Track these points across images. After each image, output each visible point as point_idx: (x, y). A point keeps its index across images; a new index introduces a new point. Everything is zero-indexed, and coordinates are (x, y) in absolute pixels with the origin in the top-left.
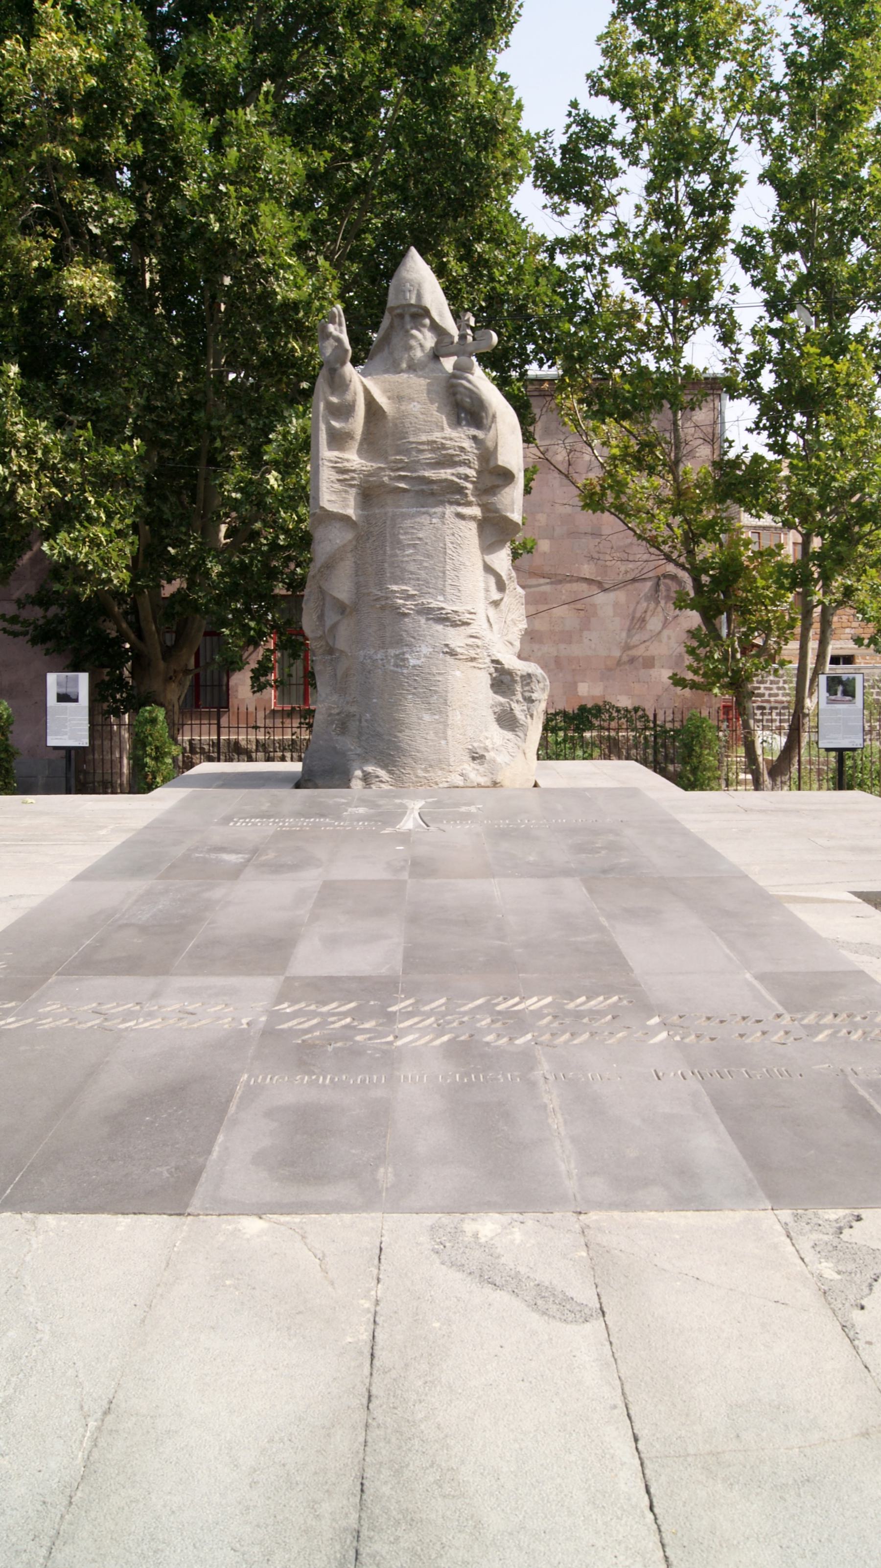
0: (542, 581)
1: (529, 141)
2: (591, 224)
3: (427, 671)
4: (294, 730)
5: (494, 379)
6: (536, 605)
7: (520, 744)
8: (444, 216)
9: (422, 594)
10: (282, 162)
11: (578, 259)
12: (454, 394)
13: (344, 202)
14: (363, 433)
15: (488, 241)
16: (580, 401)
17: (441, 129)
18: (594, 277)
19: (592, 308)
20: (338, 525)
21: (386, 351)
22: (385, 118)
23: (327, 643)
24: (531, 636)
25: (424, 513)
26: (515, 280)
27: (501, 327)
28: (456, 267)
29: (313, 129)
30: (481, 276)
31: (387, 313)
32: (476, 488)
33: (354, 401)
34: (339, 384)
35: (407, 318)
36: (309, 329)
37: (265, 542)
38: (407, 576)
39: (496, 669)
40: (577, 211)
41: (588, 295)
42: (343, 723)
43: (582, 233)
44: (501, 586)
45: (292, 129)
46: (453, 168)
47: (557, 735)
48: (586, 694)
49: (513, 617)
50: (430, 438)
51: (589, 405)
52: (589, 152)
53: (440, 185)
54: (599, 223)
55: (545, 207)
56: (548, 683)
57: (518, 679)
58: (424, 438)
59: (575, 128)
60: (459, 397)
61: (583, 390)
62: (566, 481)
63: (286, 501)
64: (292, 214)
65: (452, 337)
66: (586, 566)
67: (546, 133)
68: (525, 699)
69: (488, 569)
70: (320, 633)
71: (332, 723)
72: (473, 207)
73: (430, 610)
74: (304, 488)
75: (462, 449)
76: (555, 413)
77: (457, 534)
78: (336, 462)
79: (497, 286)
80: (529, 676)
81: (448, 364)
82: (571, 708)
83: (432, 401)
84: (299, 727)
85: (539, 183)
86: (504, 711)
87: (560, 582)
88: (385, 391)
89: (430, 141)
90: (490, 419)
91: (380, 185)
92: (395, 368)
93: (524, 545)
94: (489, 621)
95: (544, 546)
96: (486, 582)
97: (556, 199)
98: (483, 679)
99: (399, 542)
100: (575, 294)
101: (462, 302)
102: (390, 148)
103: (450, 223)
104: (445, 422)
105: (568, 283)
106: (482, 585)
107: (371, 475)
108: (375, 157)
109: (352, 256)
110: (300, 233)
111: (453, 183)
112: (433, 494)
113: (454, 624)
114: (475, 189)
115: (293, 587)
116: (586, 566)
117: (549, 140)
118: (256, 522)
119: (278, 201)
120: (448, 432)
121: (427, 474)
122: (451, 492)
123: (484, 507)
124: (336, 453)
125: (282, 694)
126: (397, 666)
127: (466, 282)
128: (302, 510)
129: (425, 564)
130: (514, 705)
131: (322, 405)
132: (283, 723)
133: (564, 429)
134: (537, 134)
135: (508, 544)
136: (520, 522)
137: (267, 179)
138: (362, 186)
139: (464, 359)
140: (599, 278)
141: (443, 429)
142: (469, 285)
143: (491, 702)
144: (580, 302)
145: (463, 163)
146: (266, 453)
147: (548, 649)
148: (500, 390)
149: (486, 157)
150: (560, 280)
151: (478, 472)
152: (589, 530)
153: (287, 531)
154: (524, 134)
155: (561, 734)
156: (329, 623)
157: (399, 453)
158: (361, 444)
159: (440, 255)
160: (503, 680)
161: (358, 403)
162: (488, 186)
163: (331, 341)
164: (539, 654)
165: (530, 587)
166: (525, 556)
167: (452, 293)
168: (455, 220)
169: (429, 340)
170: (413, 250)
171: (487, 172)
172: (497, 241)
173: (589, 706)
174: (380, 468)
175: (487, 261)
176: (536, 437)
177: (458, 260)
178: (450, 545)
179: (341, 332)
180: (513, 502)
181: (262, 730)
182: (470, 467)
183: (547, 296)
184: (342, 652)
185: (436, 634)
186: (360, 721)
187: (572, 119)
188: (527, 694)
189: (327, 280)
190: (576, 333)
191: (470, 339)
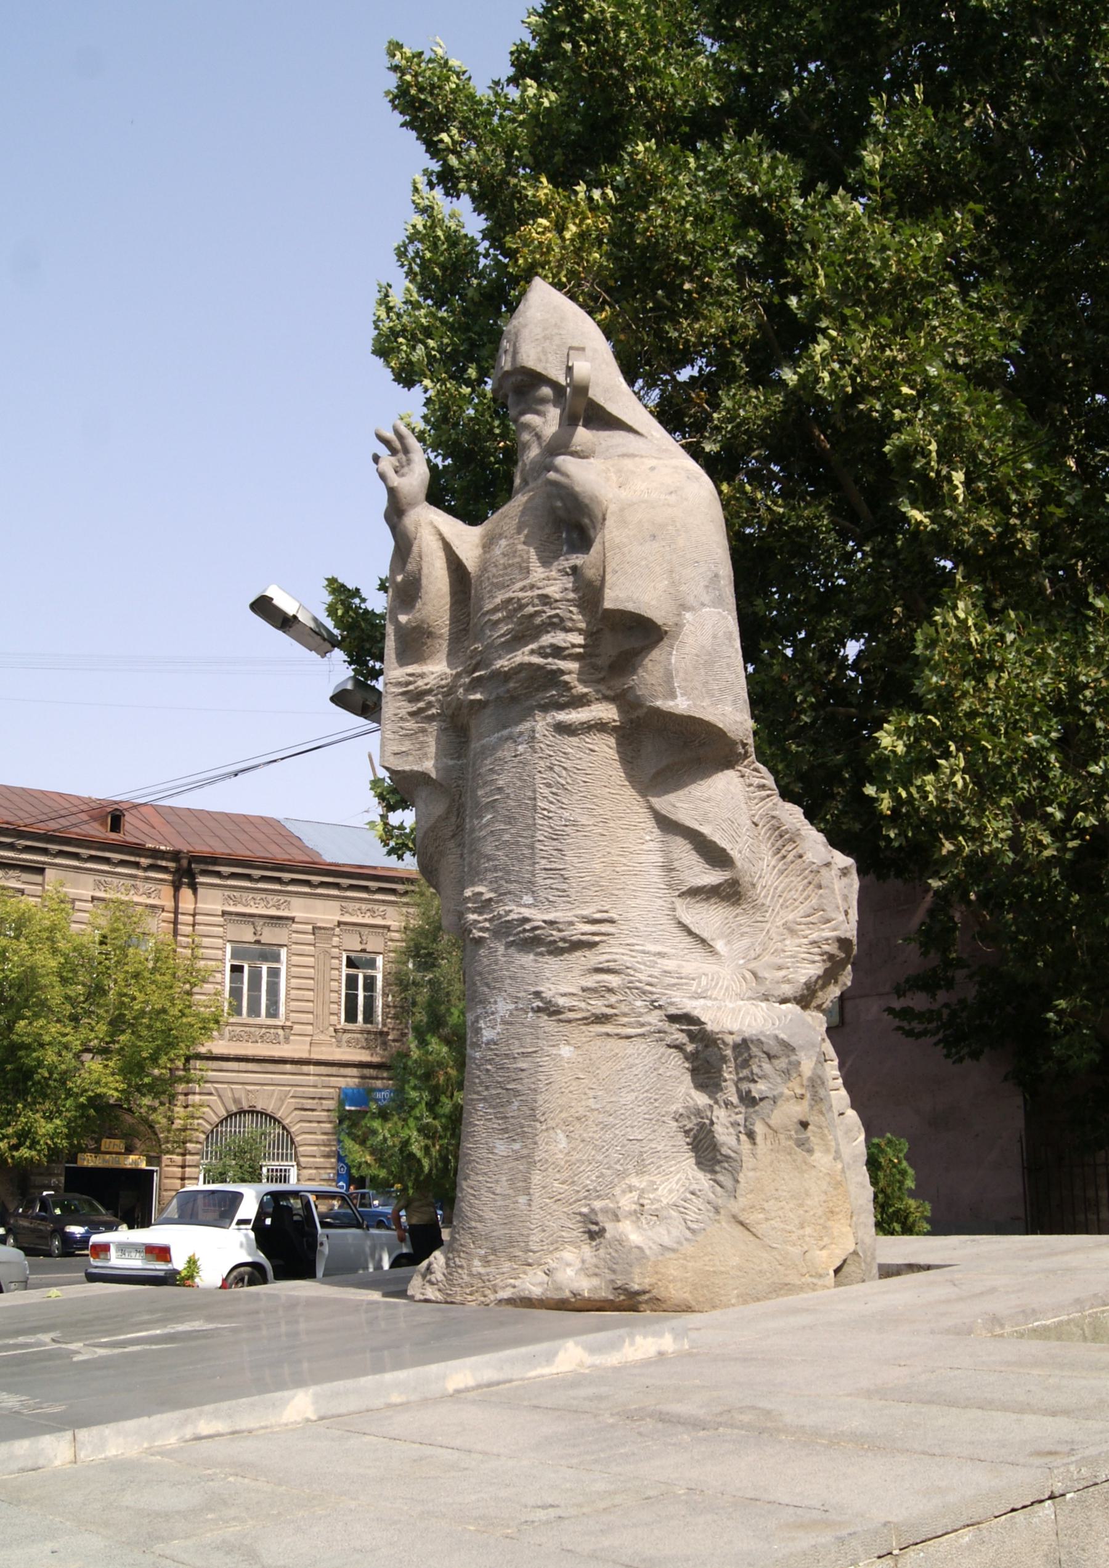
3: (504, 1050)
57: (729, 1052)
75: (545, 599)
113: (556, 950)
129: (506, 837)
178: (546, 791)
188: (744, 1086)
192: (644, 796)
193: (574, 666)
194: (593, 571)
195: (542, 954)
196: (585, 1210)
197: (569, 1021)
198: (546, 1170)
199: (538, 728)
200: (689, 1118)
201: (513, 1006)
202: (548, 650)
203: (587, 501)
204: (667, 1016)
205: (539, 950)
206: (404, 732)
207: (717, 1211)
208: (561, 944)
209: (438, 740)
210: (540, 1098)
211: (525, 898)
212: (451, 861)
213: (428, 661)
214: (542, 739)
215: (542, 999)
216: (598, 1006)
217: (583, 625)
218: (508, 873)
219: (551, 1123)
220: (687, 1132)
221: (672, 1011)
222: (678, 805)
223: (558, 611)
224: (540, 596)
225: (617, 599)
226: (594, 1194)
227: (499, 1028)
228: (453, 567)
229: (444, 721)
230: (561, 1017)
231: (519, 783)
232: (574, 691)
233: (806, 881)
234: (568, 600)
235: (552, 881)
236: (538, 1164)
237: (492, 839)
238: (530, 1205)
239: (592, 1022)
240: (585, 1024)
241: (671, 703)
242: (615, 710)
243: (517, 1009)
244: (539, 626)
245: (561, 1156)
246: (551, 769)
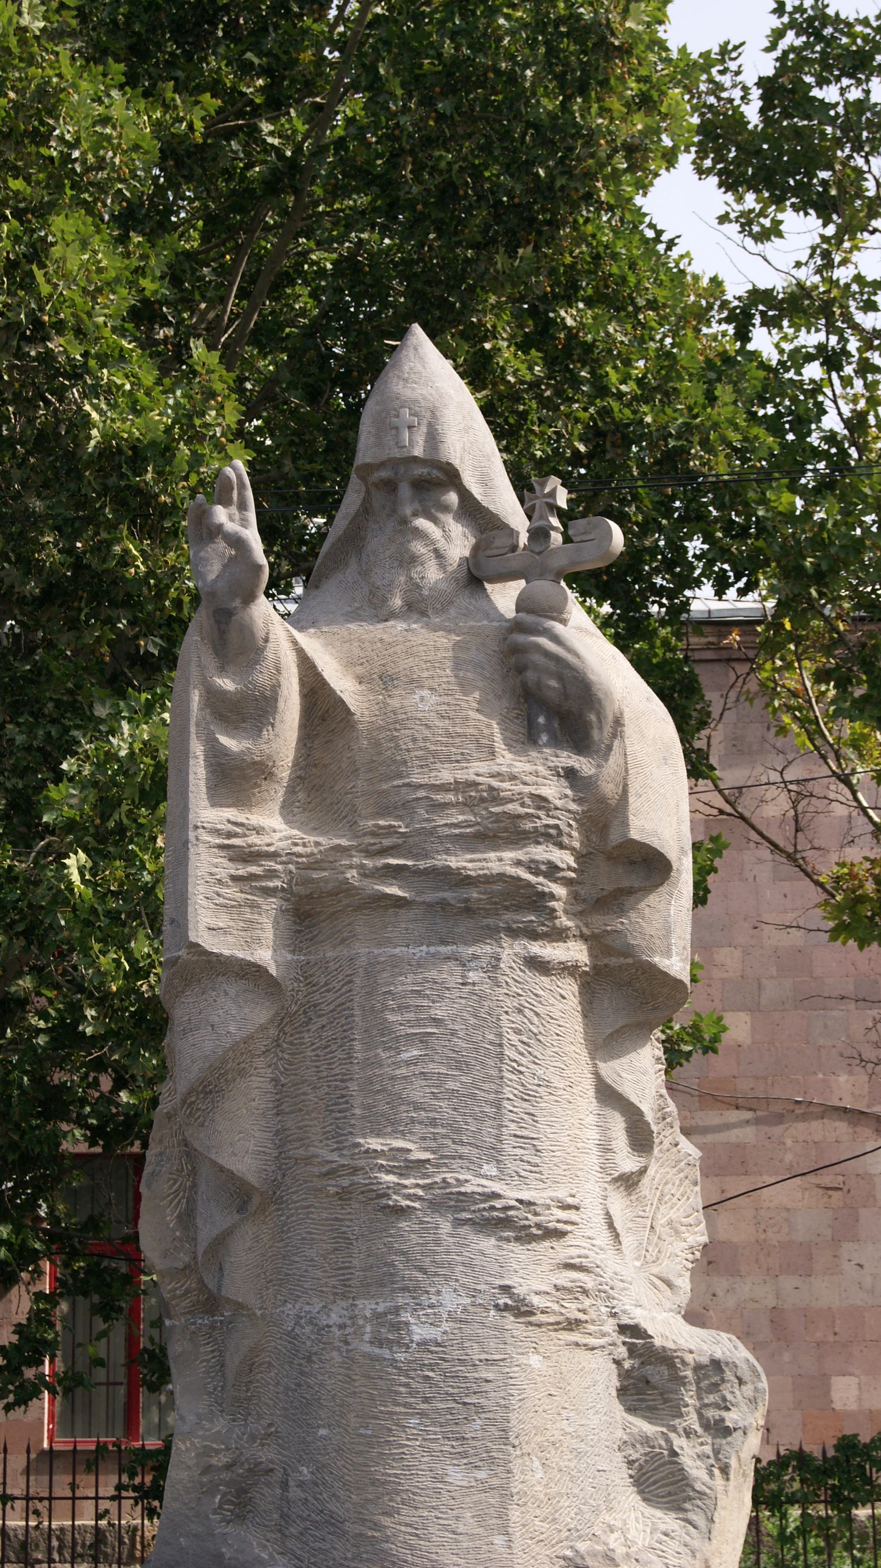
0: (734, 1116)
1: (689, 70)
2: (837, 259)
3: (456, 1354)
4: (104, 1505)
5: (605, 624)
6: (725, 1181)
7: (696, 1544)
8: (484, 245)
9: (443, 1160)
10: (105, 120)
11: (811, 339)
12: (520, 670)
13: (242, 210)
14: (296, 764)
15: (590, 302)
16: (821, 676)
17: (477, 47)
18: (847, 382)
19: (843, 453)
20: (233, 988)
21: (353, 566)
22: (339, 18)
23: (201, 1281)
24: (712, 1261)
25: (448, 958)
26: (659, 389)
27: (623, 502)
28: (518, 365)
29: (171, 47)
30: (576, 382)
31: (354, 480)
32: (575, 897)
33: (276, 687)
34: (238, 647)
35: (405, 491)
36: (166, 511)
37: (42, 1024)
38: (405, 1113)
39: (632, 1350)
40: (802, 229)
41: (831, 422)
42: (242, 1492)
43: (817, 279)
44: (641, 1138)
45: (121, 45)
46: (506, 135)
47: (784, 1516)
48: (853, 1406)
49: (673, 1214)
50: (461, 776)
51: (843, 684)
52: (830, 94)
53: (477, 174)
54: (856, 256)
55: (724, 219)
56: (764, 1384)
58: (446, 775)
59: (791, 39)
60: (531, 676)
61: (828, 651)
62: (788, 869)
63: (103, 922)
64: (123, 239)
65: (513, 533)
66: (843, 1078)
67: (724, 50)
68: (706, 1425)
69: (608, 1095)
70: (184, 1258)
71: (212, 1490)
72: (555, 224)
73: (463, 1200)
74: (149, 890)
75: (541, 801)
76: (759, 703)
77: (533, 1008)
78: (230, 835)
79: (615, 405)
80: (716, 1365)
81: (505, 597)
82: (819, 1443)
83: (465, 687)
84: (117, 1498)
85: (708, 163)
86: (652, 1457)
87: (779, 1119)
88: (349, 663)
89: (450, 75)
90: (608, 730)
91: (331, 175)
92: (376, 609)
93: (695, 1033)
94: (611, 1226)
95: (739, 1028)
96: (604, 1129)
97: (750, 200)
98: (596, 1375)
99: (385, 1029)
100: (804, 420)
101: (530, 444)
102: (355, 87)
103: (500, 260)
104: (498, 737)
105: (783, 396)
106: (593, 1135)
107: (315, 864)
108: (318, 107)
109: (265, 337)
110: (145, 283)
111: (507, 169)
112: (468, 910)
113: (525, 1236)
114: (560, 182)
115: (105, 1136)
116: (843, 1078)
117: (733, 66)
118: (20, 975)
119: (90, 209)
120: (507, 760)
121: (453, 862)
122: (516, 907)
123: (596, 942)
124: (230, 813)
125: (71, 1409)
126: (379, 1342)
127: (539, 398)
128: (141, 947)
129: (451, 1085)
130: (679, 1442)
131: (196, 698)
132: (73, 1486)
133: (780, 742)
134: (706, 55)
135: (658, 1033)
136: (686, 979)
137: (66, 158)
138: (288, 175)
139: (543, 586)
140: (858, 384)
141: (493, 754)
142: (544, 403)
143: (620, 1434)
144: (814, 439)
145: (529, 125)
146: (50, 805)
147: (753, 1290)
148: (624, 649)
149: (585, 111)
150: (765, 389)
151: (579, 857)
152: (849, 988)
153: (102, 1001)
154: (674, 55)
155: (795, 1512)
156: (206, 1233)
157: (385, 811)
158: (291, 790)
159: (475, 335)
160: (648, 1378)
161: (284, 691)
162: (590, 176)
163: (221, 544)
164: (731, 1302)
165: (705, 1130)
166: (697, 1057)
167: (504, 417)
168: (512, 253)
169: (457, 541)
170: (417, 332)
171: (587, 144)
172: (613, 300)
173: (865, 1438)
174: (337, 848)
175: (589, 348)
176: (713, 761)
177: (519, 347)
178: (514, 1038)
179: (244, 523)
180: (668, 928)
181: (19, 1505)
182: (561, 846)
183: (736, 428)
184: (240, 1306)
185: (478, 1261)
186: (285, 1485)
187: (786, 19)
188: (712, 1414)
189: (213, 395)
190: (807, 514)
191: (556, 538)
192: (593, 1058)
193: (560, 891)
194: (611, 786)
195: (508, 1240)
196: (569, 1553)
197: (539, 1325)
198: (525, 1504)
199: (504, 957)
200: (634, 1446)
201: (469, 1301)
202: (543, 867)
203: (601, 695)
204: (619, 1326)
205: (506, 1234)
206: (221, 900)
207: (693, 1553)
208: (534, 1231)
209: (276, 922)
210: (513, 1416)
211: (486, 1167)
212: (255, 1085)
213: (254, 810)
214: (508, 971)
215: (511, 1296)
216: (572, 1310)
217: (577, 845)
218: (458, 1131)
219: (526, 1449)
220: (630, 1463)
221: (625, 1321)
222: (624, 1075)
223: (557, 822)
224: (532, 796)
225: (642, 830)
226: (575, 1534)
227: (446, 1326)
228: (305, 691)
229: (287, 900)
230: (532, 1319)
231: (472, 1021)
232: (557, 922)
233: (682, 1175)
234: (569, 811)
235: (522, 1151)
236: (515, 1498)
237: (424, 1083)
238: (510, 1547)
239: (564, 1329)
240: (556, 1330)
241: (667, 962)
242: (585, 953)
243: (473, 1305)
244: (525, 832)
245: (538, 1488)
246: (520, 1011)
